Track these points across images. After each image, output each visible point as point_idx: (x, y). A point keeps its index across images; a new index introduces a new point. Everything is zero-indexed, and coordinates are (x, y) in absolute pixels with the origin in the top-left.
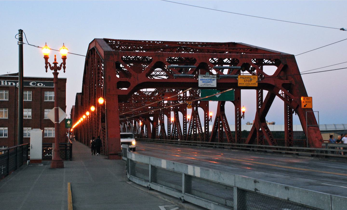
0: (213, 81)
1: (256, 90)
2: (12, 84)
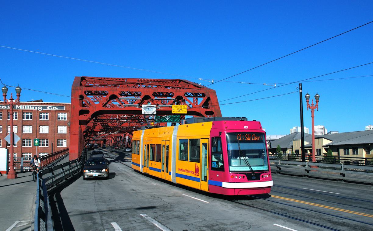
2: (35, 108)
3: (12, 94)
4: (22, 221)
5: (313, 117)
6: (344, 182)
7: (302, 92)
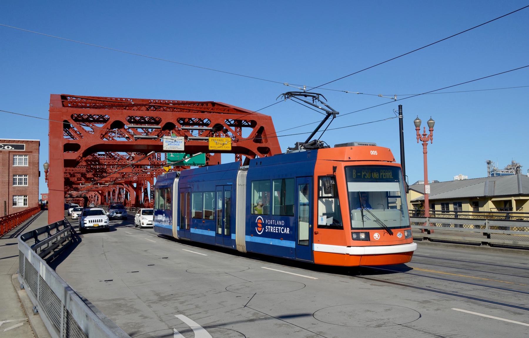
0: (181, 144)
1: (235, 162)
4: (8, 321)
5: (425, 153)
6: (489, 247)
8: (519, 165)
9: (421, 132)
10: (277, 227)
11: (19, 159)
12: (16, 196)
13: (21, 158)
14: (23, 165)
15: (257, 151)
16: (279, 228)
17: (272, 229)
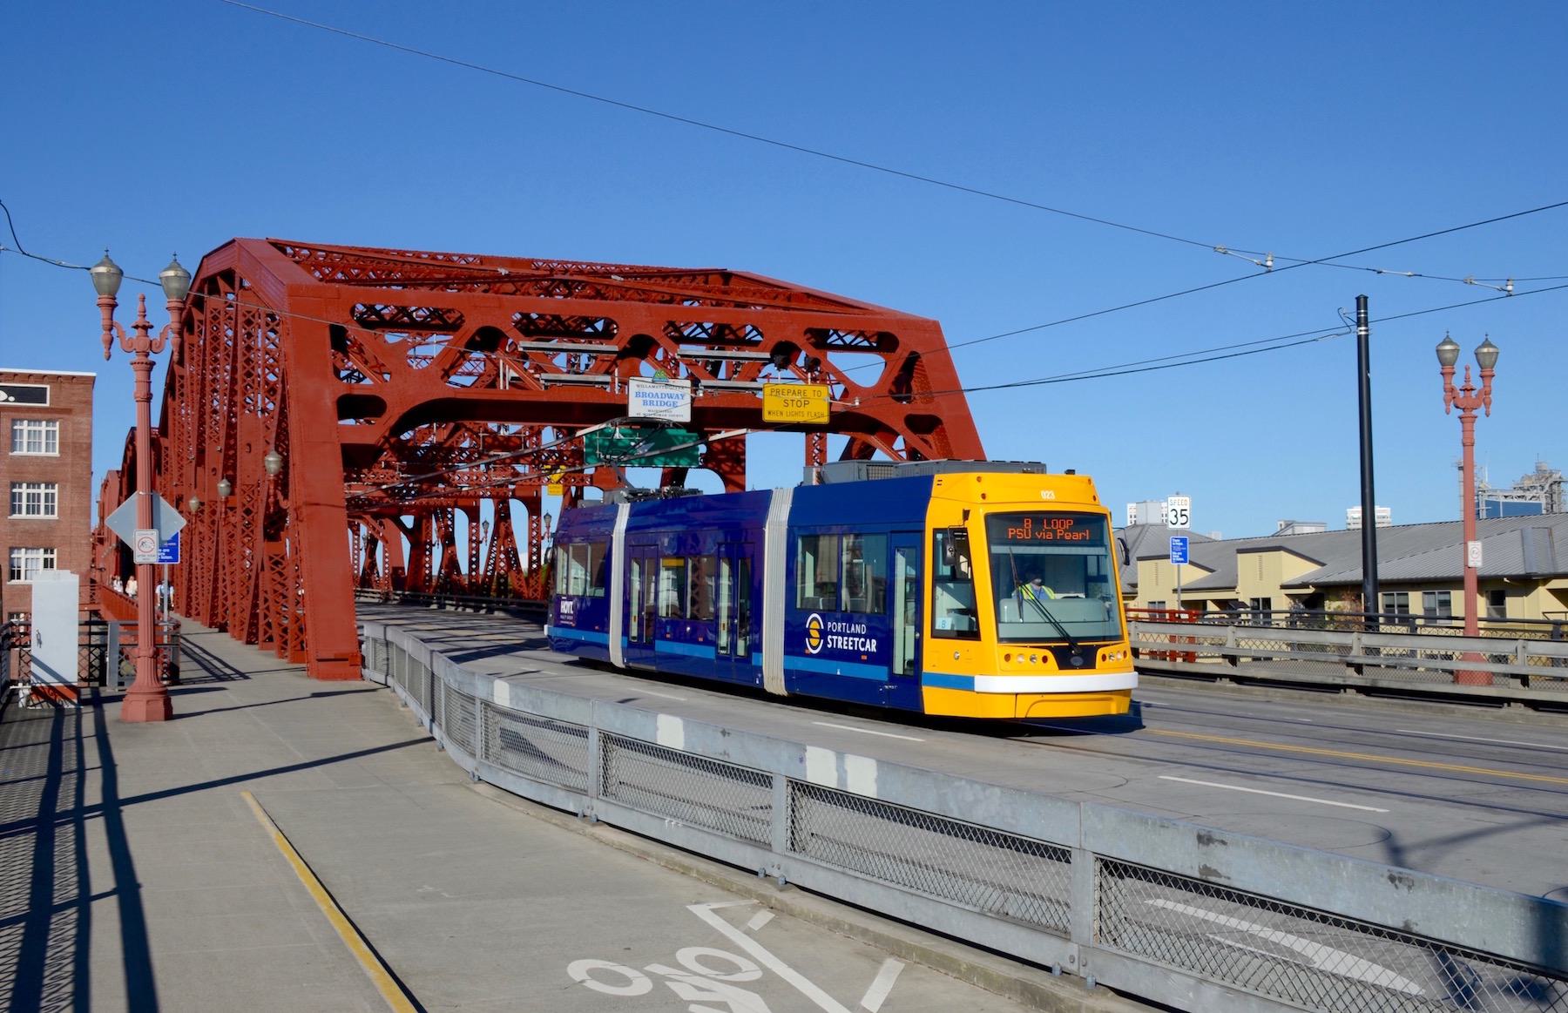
0: (680, 402)
3: (143, 299)
7: (1367, 336)
8: (1558, 476)
9: (1458, 382)
10: (851, 639)
11: (29, 431)
12: (19, 548)
13: (37, 428)
14: (43, 453)
15: (905, 427)
16: (856, 639)
17: (840, 643)
